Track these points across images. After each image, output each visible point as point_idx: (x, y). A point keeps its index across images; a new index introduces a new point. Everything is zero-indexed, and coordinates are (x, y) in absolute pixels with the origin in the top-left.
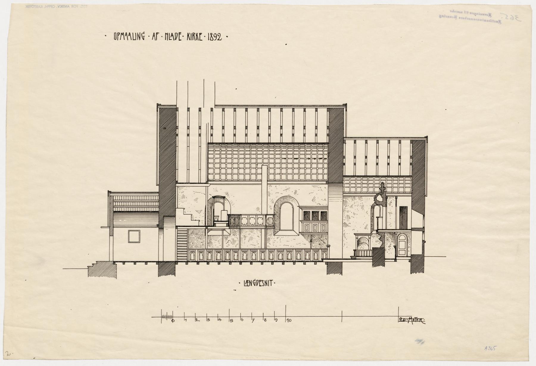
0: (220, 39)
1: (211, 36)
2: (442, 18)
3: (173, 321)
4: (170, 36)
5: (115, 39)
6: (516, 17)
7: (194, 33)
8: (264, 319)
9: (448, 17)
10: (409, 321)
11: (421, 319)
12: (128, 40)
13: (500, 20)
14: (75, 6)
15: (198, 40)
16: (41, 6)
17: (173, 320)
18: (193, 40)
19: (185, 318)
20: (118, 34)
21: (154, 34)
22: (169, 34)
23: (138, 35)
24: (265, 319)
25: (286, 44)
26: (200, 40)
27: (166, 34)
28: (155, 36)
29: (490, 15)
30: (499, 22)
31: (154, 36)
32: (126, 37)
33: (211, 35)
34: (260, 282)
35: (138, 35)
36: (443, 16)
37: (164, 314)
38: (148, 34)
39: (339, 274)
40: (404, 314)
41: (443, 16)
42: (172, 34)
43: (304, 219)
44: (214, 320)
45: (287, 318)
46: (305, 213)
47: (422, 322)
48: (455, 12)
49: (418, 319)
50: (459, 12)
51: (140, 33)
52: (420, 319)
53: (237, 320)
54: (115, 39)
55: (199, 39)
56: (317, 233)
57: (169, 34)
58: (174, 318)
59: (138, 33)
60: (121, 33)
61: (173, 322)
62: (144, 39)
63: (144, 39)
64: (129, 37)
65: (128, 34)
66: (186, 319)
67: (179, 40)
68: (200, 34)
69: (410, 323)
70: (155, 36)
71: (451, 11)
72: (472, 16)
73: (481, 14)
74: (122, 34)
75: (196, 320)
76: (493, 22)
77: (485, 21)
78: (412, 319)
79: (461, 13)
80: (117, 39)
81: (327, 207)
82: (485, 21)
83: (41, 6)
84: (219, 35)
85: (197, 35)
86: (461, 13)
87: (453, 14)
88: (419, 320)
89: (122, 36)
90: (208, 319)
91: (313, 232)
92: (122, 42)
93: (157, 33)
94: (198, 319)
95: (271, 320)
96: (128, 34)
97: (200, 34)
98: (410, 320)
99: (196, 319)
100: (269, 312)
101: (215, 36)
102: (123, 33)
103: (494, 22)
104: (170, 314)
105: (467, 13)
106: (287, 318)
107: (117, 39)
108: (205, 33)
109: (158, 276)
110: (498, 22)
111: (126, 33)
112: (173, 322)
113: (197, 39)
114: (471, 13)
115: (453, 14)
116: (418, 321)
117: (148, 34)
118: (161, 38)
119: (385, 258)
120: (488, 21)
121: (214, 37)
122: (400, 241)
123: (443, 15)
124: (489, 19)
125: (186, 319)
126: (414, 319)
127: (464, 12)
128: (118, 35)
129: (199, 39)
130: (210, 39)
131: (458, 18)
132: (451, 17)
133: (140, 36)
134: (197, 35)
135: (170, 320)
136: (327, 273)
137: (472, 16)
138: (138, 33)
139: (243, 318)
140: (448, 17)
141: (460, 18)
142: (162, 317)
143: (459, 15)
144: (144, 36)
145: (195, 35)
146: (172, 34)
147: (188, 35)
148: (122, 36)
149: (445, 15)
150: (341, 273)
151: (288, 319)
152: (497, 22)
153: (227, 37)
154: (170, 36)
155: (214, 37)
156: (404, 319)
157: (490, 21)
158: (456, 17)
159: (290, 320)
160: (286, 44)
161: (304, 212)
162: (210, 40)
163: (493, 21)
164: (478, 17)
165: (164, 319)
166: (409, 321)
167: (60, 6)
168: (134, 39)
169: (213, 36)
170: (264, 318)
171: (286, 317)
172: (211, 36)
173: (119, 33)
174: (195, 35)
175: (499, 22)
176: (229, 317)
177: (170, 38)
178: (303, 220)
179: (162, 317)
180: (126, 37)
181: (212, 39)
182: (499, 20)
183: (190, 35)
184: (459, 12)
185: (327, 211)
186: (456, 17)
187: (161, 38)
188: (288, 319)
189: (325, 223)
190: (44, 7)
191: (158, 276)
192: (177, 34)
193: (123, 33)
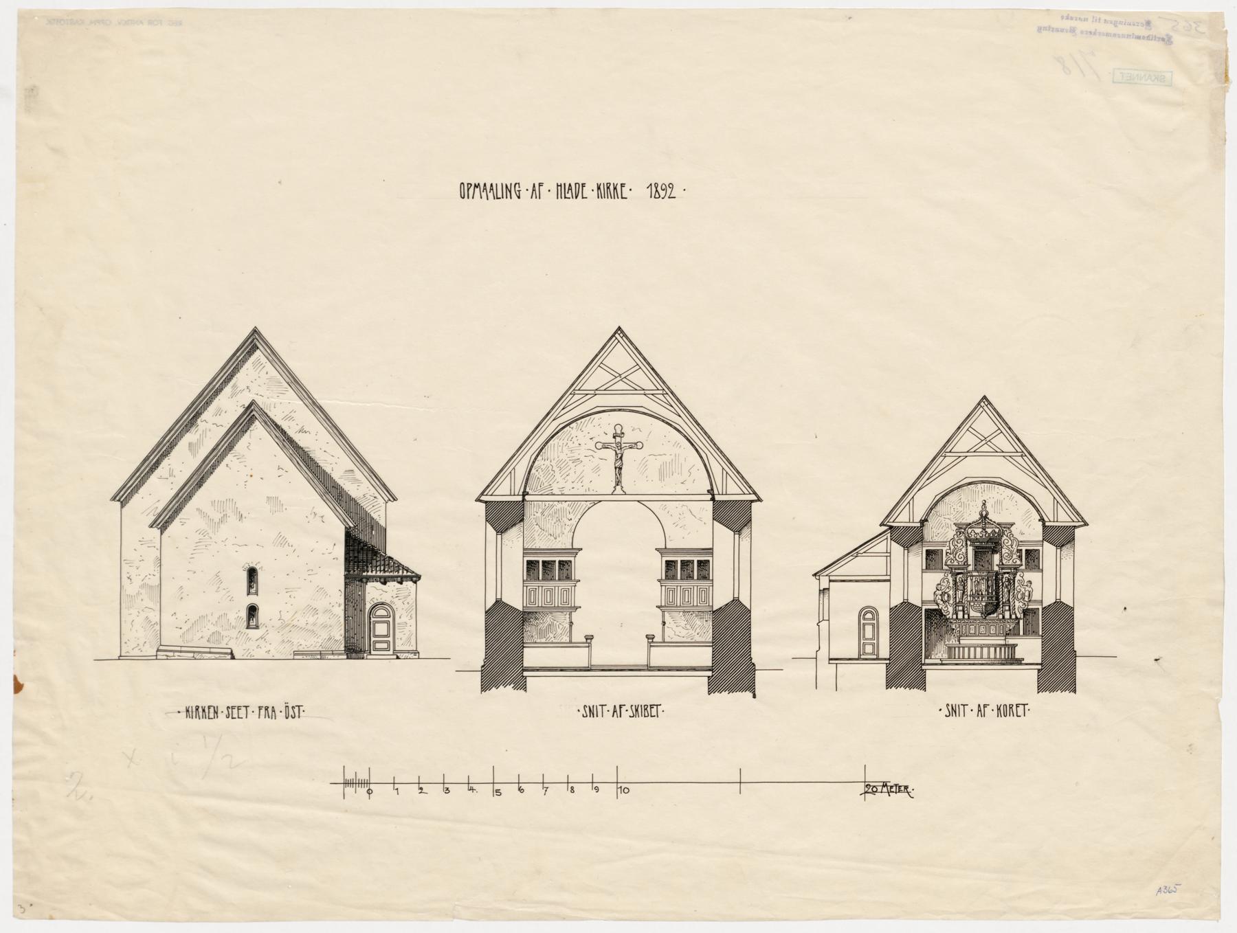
1: (657, 191)
3: (371, 792)
4: (566, 191)
8: (570, 789)
9: (1057, 30)
11: (906, 787)
17: (369, 789)
19: (396, 786)
24: (572, 788)
26: (622, 198)
27: (558, 186)
28: (536, 191)
31: (571, 189)
32: (484, 194)
33: (656, 188)
34: (651, 708)
37: (350, 776)
39: (727, 692)
40: (875, 776)
42: (570, 185)
43: (926, 569)
44: (459, 791)
46: (670, 565)
48: (1072, 19)
53: (510, 791)
55: (620, 196)
56: (552, 607)
57: (565, 184)
58: (372, 787)
60: (475, 184)
62: (519, 197)
63: (519, 197)
64: (491, 195)
65: (488, 187)
66: (397, 789)
67: (583, 198)
68: (623, 185)
70: (536, 191)
74: (476, 186)
75: (520, 790)
78: (889, 788)
81: (710, 551)
84: (671, 186)
86: (1086, 20)
87: (1068, 24)
88: (902, 788)
89: (477, 190)
90: (498, 791)
91: (543, 605)
92: (477, 202)
93: (540, 185)
96: (488, 187)
97: (623, 185)
99: (421, 789)
100: (531, 773)
101: (664, 187)
104: (363, 776)
106: (619, 785)
109: (1038, 692)
113: (615, 196)
115: (1068, 24)
117: (526, 185)
118: (549, 196)
119: (526, 664)
122: (865, 622)
125: (397, 789)
126: (891, 787)
129: (620, 196)
132: (1062, 30)
133: (510, 190)
134: (615, 188)
135: (362, 791)
136: (709, 692)
137: (1110, 29)
139: (475, 786)
140: (1057, 30)
141: (1082, 32)
142: (347, 783)
143: (1081, 26)
144: (519, 191)
146: (570, 185)
150: (925, 689)
152: (1163, 40)
154: (566, 191)
156: (874, 786)
158: (1073, 30)
161: (927, 551)
162: (655, 197)
163: (1155, 36)
169: (659, 189)
170: (570, 785)
171: (740, 783)
172: (657, 191)
176: (494, 783)
177: (567, 196)
178: (664, 578)
179: (347, 783)
181: (657, 196)
183: (602, 187)
185: (572, 559)
186: (1073, 30)
187: (549, 196)
189: (565, 584)
191: (1038, 692)
193: (479, 184)
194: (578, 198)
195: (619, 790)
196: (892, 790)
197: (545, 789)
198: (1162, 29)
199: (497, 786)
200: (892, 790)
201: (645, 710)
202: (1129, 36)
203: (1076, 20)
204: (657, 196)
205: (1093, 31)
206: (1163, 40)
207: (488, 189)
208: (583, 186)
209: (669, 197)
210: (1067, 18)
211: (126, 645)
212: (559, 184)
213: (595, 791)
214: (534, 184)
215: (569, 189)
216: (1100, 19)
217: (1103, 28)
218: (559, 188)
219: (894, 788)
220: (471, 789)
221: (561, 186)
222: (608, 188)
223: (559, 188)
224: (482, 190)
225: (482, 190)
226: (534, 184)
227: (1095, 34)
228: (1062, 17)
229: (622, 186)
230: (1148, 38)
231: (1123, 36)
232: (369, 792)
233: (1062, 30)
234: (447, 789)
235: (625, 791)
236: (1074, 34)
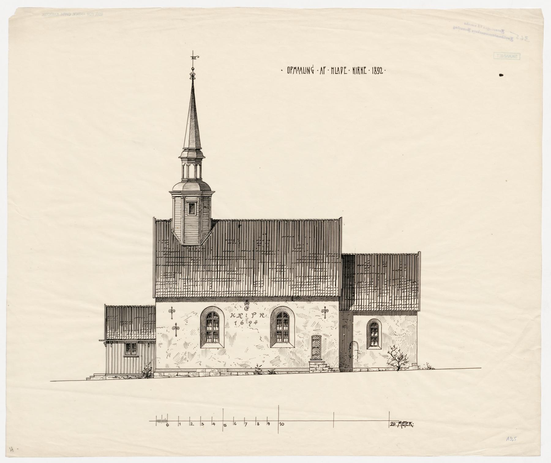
0: (382, 73)
1: (375, 70)
5: (289, 72)
7: (359, 67)
10: (398, 426)
11: (410, 423)
15: (360, 74)
20: (292, 68)
21: (321, 68)
23: (308, 69)
25: (501, 75)
26: (365, 73)
27: (332, 68)
28: (322, 70)
32: (298, 72)
33: (375, 69)
35: (308, 69)
38: (317, 68)
45: (279, 422)
47: (411, 426)
48: (469, 25)
49: (408, 422)
52: (410, 422)
53: (208, 424)
54: (289, 72)
55: (364, 73)
58: (169, 423)
61: (167, 426)
62: (313, 73)
63: (313, 73)
64: (301, 72)
66: (180, 423)
69: (400, 427)
70: (322, 70)
71: (465, 24)
74: (295, 68)
80: (290, 73)
82: (497, 36)
85: (362, 70)
88: (408, 424)
89: (295, 70)
90: (202, 423)
93: (324, 68)
94: (194, 423)
95: (263, 424)
97: (365, 68)
98: (400, 425)
102: (296, 67)
107: (290, 73)
108: (350, 67)
111: (298, 67)
112: (167, 426)
116: (408, 425)
117: (317, 68)
121: (377, 70)
128: (291, 69)
129: (364, 73)
130: (374, 73)
132: (464, 29)
134: (362, 70)
144: (313, 70)
145: (360, 69)
147: (354, 69)
148: (295, 70)
151: (280, 423)
153: (349, 70)
155: (377, 70)
159: (283, 424)
160: (501, 75)
163: (505, 37)
165: (157, 423)
166: (398, 426)
168: (305, 72)
172: (375, 70)
174: (360, 69)
181: (376, 73)
183: (355, 69)
186: (469, 30)
188: (280, 423)
192: (289, 67)
193: (296, 67)
195: (280, 424)
196: (407, 424)
197: (245, 424)
199: (225, 423)
200: (407, 424)
203: (471, 25)
204: (376, 73)
207: (299, 70)
209: (381, 73)
210: (467, 24)
213: (268, 425)
214: (321, 68)
218: (333, 69)
219: (404, 423)
220: (235, 424)
221: (333, 68)
222: (358, 70)
223: (333, 69)
224: (300, 70)
225: (300, 70)
226: (321, 68)
227: (478, 32)
229: (364, 68)
232: (167, 425)
233: (464, 29)
234: (202, 423)
235: (282, 424)
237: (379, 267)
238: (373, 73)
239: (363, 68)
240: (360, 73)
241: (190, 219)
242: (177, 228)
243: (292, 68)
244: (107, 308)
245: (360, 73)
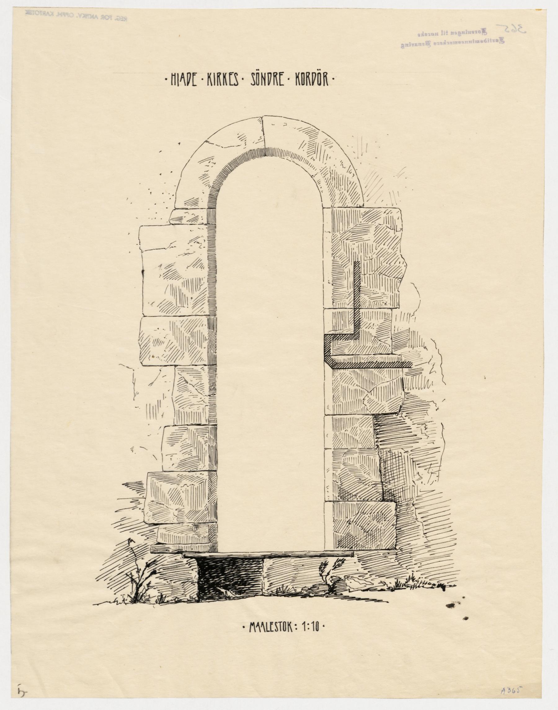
2: (406, 48)
6: (519, 27)
9: (416, 45)
12: (320, 161)
13: (501, 36)
14: (37, 13)
16: (51, 12)
18: (265, 74)
20: (308, 74)
22: (178, 74)
26: (280, 85)
27: (172, 75)
29: (484, 30)
30: (501, 40)
31: (184, 78)
32: (257, 629)
35: (262, 76)
36: (407, 45)
41: (407, 45)
42: (183, 74)
48: (426, 35)
50: (433, 34)
51: (288, 631)
57: (178, 74)
59: (262, 73)
64: (262, 629)
65: (260, 624)
71: (419, 35)
72: (456, 38)
73: (470, 33)
76: (474, 43)
77: (478, 42)
79: (437, 34)
82: (478, 42)
83: (50, 13)
85: (224, 77)
86: (437, 34)
87: (423, 40)
96: (260, 624)
97: (281, 74)
103: (492, 41)
105: (446, 34)
108: (290, 74)
110: (499, 40)
114: (452, 33)
115: (423, 40)
120: (482, 42)
123: (408, 43)
124: (483, 39)
127: (440, 33)
131: (432, 44)
132: (420, 44)
134: (224, 77)
137: (456, 38)
138: (262, 73)
140: (416, 45)
141: (435, 44)
143: (432, 39)
149: (410, 43)
152: (497, 41)
157: (485, 41)
158: (428, 43)
164: (465, 37)
167: (83, 16)
173: (309, 73)
175: (501, 40)
180: (257, 629)
182: (500, 38)
183: (212, 76)
184: (433, 34)
186: (428, 43)
190: (57, 16)
194: (189, 84)
198: (493, 34)
201: (164, 274)
202: (470, 42)
205: (443, 41)
206: (497, 41)
208: (193, 75)
210: (423, 35)
211: (239, 133)
212: (174, 74)
215: (182, 78)
216: (447, 32)
217: (450, 38)
218: (174, 77)
221: (175, 75)
223: (174, 77)
227: (445, 43)
228: (419, 35)
230: (485, 41)
231: (466, 42)
236: (429, 46)
237: (338, 426)
238: (172, 84)
239: (300, 74)
240: (222, 83)
241: (175, 496)
242: (183, 541)
243: (275, 74)
244: (540, 697)
245: (222, 83)
